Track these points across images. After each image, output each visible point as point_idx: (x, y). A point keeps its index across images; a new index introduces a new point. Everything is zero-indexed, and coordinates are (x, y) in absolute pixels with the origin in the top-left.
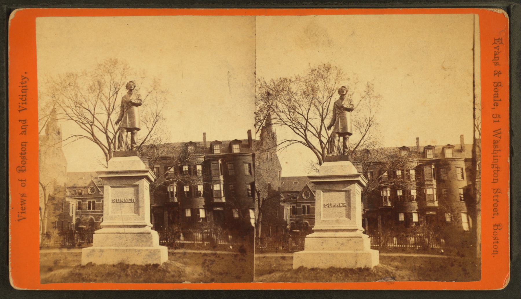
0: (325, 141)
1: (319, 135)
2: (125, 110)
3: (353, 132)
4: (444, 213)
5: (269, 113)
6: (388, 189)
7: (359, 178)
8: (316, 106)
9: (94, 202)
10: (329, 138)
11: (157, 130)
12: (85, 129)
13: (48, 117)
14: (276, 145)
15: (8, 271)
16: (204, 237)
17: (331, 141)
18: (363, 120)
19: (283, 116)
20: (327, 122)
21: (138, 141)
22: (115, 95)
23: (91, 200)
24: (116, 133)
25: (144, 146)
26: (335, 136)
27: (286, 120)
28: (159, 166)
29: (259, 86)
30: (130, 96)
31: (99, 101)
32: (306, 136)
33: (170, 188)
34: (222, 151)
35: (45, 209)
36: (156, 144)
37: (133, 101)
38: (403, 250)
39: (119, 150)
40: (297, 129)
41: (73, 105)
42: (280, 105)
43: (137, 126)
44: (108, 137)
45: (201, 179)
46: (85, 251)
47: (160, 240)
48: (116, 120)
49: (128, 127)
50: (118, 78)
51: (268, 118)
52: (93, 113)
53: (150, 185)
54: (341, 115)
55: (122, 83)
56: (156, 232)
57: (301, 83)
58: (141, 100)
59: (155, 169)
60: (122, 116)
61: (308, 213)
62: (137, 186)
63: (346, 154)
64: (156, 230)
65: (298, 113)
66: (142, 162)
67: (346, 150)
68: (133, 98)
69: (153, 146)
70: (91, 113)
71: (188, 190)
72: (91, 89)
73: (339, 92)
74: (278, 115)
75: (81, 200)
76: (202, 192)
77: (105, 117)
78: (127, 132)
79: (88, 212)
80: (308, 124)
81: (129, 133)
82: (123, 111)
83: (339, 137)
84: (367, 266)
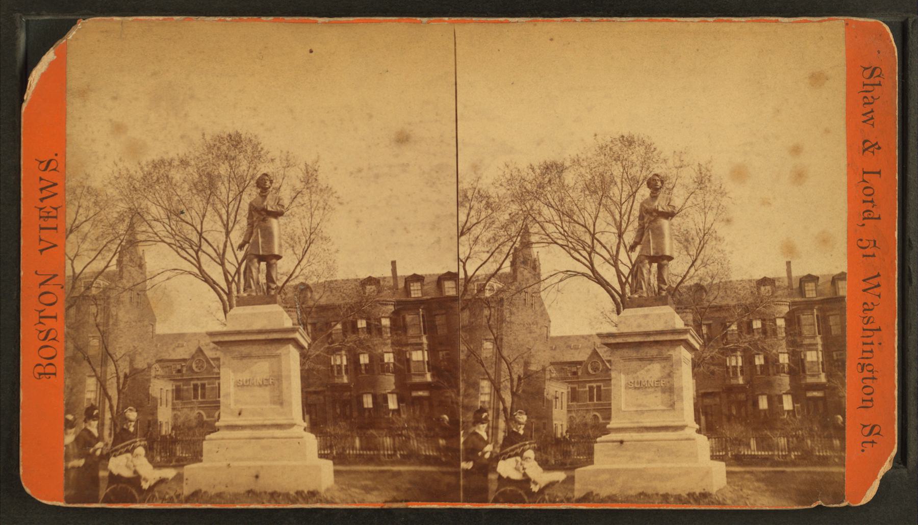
0: (625, 271)
1: (615, 261)
2: (255, 224)
3: (283, 254)
4: (758, 395)
5: (526, 226)
6: (739, 353)
7: (688, 337)
8: (217, 211)
9: (599, 387)
10: (633, 266)
11: (312, 257)
12: (185, 259)
13: (122, 237)
14: (539, 282)
16: (397, 445)
17: (637, 271)
18: (299, 232)
19: (550, 228)
20: (629, 237)
21: (674, 278)
23: (199, 383)
24: (240, 265)
25: (290, 286)
26: (641, 262)
27: (163, 233)
28: (711, 322)
29: (508, 176)
30: (263, 202)
31: (210, 208)
32: (592, 264)
33: (730, 361)
34: (818, 293)
35: (119, 398)
36: (310, 282)
37: (269, 209)
38: (370, 460)
39: (245, 295)
40: (183, 249)
41: (163, 214)
42: (155, 211)
44: (226, 273)
45: (784, 343)
46: (190, 469)
47: (320, 449)
48: (240, 241)
49: (261, 253)
50: (635, 171)
51: (525, 232)
52: (199, 230)
53: (301, 356)
54: (263, 224)
55: (642, 178)
57: (583, 170)
58: (283, 206)
59: (309, 327)
60: (250, 234)
61: (599, 399)
62: (278, 356)
63: (664, 293)
64: (312, 432)
65: (184, 221)
66: (286, 315)
67: (663, 286)
68: (270, 205)
69: (699, 288)
70: (196, 229)
71: (367, 361)
72: (589, 188)
73: (649, 185)
74: (542, 227)
76: (391, 365)
77: (614, 239)
78: (650, 264)
79: (588, 405)
80: (595, 241)
81: (263, 265)
82: (251, 225)
83: (259, 263)
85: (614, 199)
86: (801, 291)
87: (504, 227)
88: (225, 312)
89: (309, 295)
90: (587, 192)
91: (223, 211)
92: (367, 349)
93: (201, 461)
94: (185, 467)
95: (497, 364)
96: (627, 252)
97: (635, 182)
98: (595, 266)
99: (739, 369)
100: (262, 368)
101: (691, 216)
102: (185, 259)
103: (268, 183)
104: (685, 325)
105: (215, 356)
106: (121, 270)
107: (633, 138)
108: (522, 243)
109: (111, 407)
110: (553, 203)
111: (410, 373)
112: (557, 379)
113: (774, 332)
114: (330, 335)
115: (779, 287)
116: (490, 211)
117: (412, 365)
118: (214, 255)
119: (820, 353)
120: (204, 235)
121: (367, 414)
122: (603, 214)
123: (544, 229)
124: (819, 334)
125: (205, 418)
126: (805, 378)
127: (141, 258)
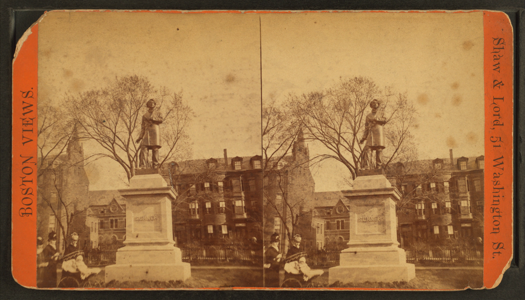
0: (358, 155)
1: (351, 149)
2: (146, 128)
3: (162, 145)
4: (433, 226)
5: (301, 129)
6: (422, 202)
7: (393, 192)
8: (124, 120)
9: (342, 221)
10: (362, 152)
11: (178, 147)
12: (106, 148)
13: (70, 136)
14: (308, 161)
15: (309, 291)
16: (227, 254)
17: (364, 155)
18: (171, 133)
19: (315, 130)
20: (360, 135)
21: (385, 159)
22: (361, 113)
23: (114, 219)
24: (137, 151)
25: (166, 164)
26: (367, 150)
27: (93, 133)
29: (291, 101)
31: (120, 119)
32: (339, 151)
33: (418, 206)
35: (68, 228)
36: (177, 161)
37: (154, 119)
38: (211, 263)
39: (140, 168)
40: (105, 142)
42: (88, 120)
43: (158, 144)
45: (448, 196)
46: (109, 268)
47: (183, 257)
48: (137, 138)
49: (149, 144)
50: (363, 98)
51: (300, 133)
53: (172, 203)
56: (179, 249)
57: (333, 97)
58: (162, 118)
59: (177, 187)
60: (143, 133)
61: (343, 228)
62: (159, 203)
63: (380, 168)
64: (178, 247)
65: (105, 126)
66: (163, 180)
67: (379, 163)
68: (154, 117)
69: (400, 164)
71: (210, 206)
72: (337, 108)
74: (310, 130)
75: (329, 220)
76: (224, 209)
77: (351, 137)
78: (148, 150)
79: (336, 232)
80: (340, 138)
81: (151, 151)
82: (143, 128)
84: (404, 280)
85: (351, 114)
86: (458, 166)
87: (288, 130)
88: (129, 178)
89: (177, 168)
90: (336, 110)
91: (128, 121)
92: (210, 200)
93: (115, 263)
94: (106, 267)
95: (284, 208)
96: (359, 144)
97: (363, 104)
98: (341, 152)
99: (196, 210)
100: (150, 210)
101: (395, 124)
102: (106, 148)
103: (153, 104)
104: (392, 186)
105: (123, 204)
106: (69, 155)
107: (362, 79)
108: (298, 139)
109: (64, 233)
110: (316, 116)
111: (234, 213)
112: (319, 217)
113: (443, 190)
114: (189, 191)
115: (445, 164)
116: (280, 121)
117: (236, 208)
118: (122, 146)
119: (469, 202)
120: (117, 134)
121: (210, 236)
122: (345, 122)
123: (311, 131)
124: (469, 191)
125: (117, 239)
126: (460, 216)
127: (80, 148)
